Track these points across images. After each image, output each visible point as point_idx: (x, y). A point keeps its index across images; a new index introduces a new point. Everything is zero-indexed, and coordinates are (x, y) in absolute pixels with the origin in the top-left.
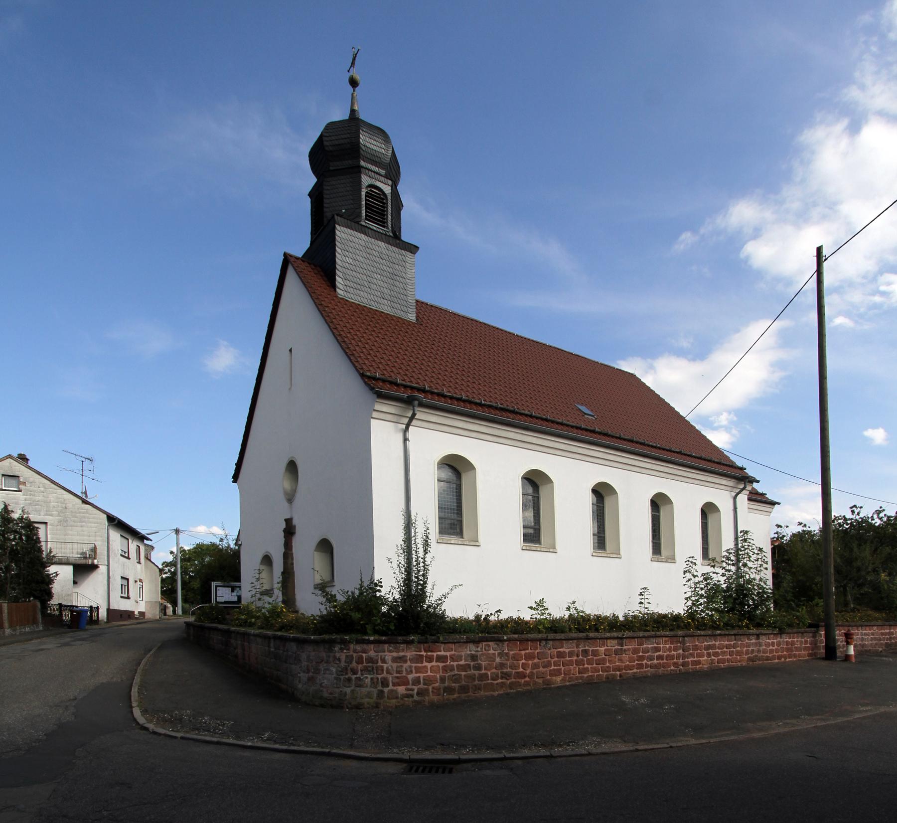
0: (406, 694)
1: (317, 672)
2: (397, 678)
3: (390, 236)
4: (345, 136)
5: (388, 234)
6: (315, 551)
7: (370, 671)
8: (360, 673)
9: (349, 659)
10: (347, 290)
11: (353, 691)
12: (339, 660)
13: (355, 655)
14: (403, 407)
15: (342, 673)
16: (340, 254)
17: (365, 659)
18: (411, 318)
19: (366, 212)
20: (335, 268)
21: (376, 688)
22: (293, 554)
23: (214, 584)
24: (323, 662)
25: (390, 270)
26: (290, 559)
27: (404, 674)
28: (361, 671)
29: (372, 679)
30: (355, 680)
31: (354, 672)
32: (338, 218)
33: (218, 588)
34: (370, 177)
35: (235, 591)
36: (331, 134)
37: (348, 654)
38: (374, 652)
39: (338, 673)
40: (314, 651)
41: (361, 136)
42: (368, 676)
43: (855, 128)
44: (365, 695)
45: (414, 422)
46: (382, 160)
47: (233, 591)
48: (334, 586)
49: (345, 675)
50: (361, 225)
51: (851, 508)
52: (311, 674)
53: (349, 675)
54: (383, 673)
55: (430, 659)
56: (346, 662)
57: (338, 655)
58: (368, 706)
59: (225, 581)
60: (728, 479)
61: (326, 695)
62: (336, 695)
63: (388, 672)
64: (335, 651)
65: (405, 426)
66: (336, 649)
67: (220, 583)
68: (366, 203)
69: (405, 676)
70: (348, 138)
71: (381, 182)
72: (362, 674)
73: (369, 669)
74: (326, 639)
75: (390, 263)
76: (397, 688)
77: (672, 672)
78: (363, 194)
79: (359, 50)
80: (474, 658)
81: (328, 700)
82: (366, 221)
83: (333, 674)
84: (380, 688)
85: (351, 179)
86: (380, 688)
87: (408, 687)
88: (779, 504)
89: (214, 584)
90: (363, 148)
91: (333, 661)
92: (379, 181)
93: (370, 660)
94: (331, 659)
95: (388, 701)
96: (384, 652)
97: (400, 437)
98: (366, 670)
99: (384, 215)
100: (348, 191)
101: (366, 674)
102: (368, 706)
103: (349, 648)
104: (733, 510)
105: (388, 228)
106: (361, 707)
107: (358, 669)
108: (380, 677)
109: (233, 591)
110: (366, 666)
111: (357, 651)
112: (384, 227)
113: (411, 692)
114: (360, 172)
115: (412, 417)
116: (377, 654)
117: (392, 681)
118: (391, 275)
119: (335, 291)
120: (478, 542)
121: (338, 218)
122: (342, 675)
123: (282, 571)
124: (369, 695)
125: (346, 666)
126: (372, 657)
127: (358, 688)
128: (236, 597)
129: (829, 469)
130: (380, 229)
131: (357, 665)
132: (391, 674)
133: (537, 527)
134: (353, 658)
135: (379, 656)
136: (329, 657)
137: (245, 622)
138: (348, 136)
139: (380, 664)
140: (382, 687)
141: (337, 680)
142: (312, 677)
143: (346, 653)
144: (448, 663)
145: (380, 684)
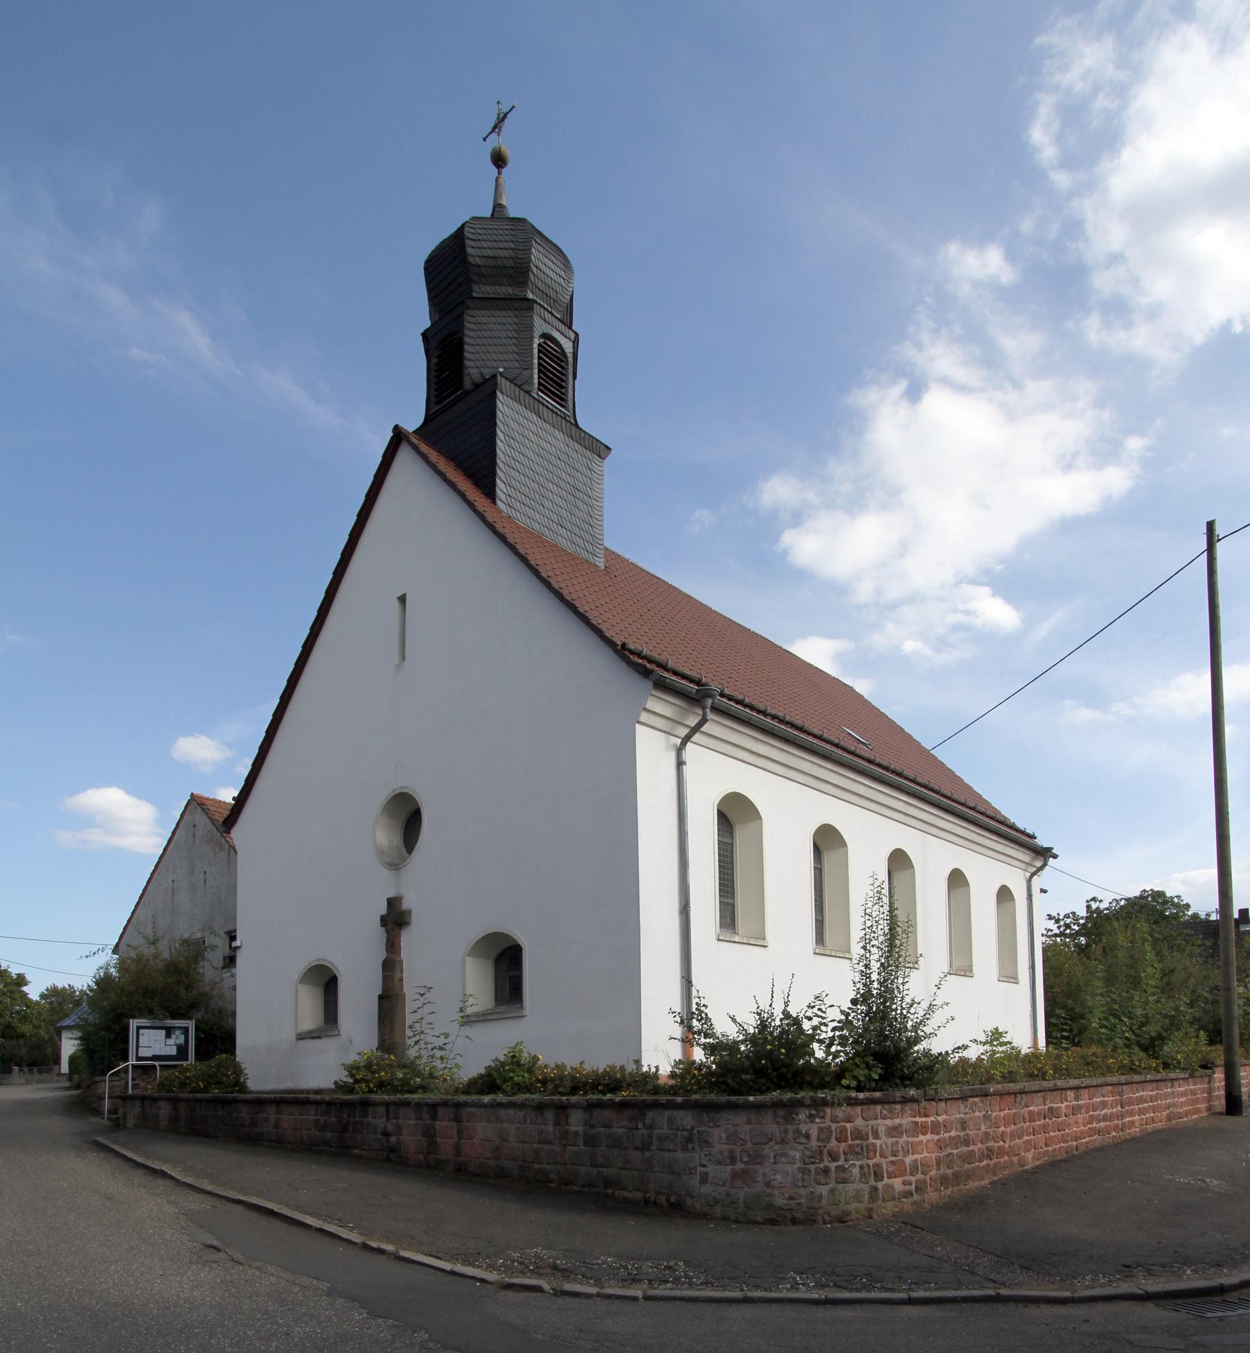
0: (904, 1190)
1: (758, 1161)
2: (893, 1163)
3: (572, 424)
4: (506, 245)
5: (568, 418)
6: (469, 955)
7: (858, 1153)
8: (842, 1158)
9: (825, 1134)
10: (511, 505)
11: (832, 1191)
12: (807, 1136)
13: (834, 1126)
14: (675, 705)
15: (813, 1160)
16: (502, 442)
17: (851, 1132)
18: (597, 564)
19: (539, 377)
20: (493, 463)
21: (868, 1183)
22: (402, 961)
23: (134, 1023)
24: (773, 1143)
25: (571, 481)
26: (398, 973)
27: (900, 1157)
28: (845, 1154)
29: (861, 1167)
30: (836, 1171)
31: (834, 1157)
33: (141, 1031)
34: (545, 320)
35: (173, 1036)
36: (480, 237)
37: (822, 1125)
38: (861, 1119)
39: (806, 1160)
40: (749, 1122)
41: (533, 249)
42: (856, 1162)
43: (915, 393)
44: (852, 1197)
45: (697, 737)
46: (560, 296)
47: (168, 1036)
48: (524, 1016)
49: (820, 1163)
51: (1087, 901)
52: (739, 1166)
53: (826, 1163)
54: (876, 1157)
55: (924, 1129)
56: (819, 1139)
57: (804, 1128)
58: (858, 1215)
59: (154, 1018)
60: (1026, 852)
61: (779, 1201)
62: (803, 1201)
63: (883, 1155)
64: (800, 1120)
65: (680, 740)
66: (800, 1117)
67: (145, 1021)
68: (539, 364)
69: (901, 1160)
70: (512, 249)
71: (559, 331)
72: (846, 1160)
73: (857, 1150)
74: (785, 1100)
75: (571, 469)
76: (893, 1182)
77: (1115, 1140)
78: (535, 346)
79: (513, 107)
80: (963, 1124)
81: (786, 1210)
82: (540, 393)
83: (796, 1164)
84: (872, 1182)
85: (514, 319)
86: (872, 1182)
87: (906, 1178)
89: (134, 1023)
90: (534, 269)
91: (795, 1140)
92: (557, 330)
93: (858, 1135)
94: (790, 1136)
95: (883, 1204)
96: (876, 1119)
97: (671, 758)
98: (852, 1152)
99: (562, 387)
100: (510, 338)
101: (852, 1160)
102: (858, 1215)
103: (825, 1113)
104: (1027, 898)
105: (569, 411)
106: (846, 1219)
107: (839, 1150)
108: (871, 1162)
109: (168, 1036)
110: (852, 1145)
111: (838, 1119)
112: (562, 406)
113: (908, 1187)
114: (531, 309)
115: (696, 729)
116: (866, 1123)
117: (887, 1170)
118: (572, 488)
119: (494, 502)
120: (765, 939)
122: (813, 1163)
123: (380, 992)
124: (857, 1197)
125: (820, 1147)
126: (860, 1128)
127: (841, 1185)
128: (175, 1048)
129: (1229, 837)
131: (838, 1144)
133: (820, 918)
134: (831, 1132)
135: (870, 1127)
136: (786, 1131)
137: (405, 1082)
138: (512, 245)
139: (871, 1140)
140: (875, 1181)
141: (803, 1173)
142: (745, 1171)
143: (819, 1123)
145: (873, 1176)
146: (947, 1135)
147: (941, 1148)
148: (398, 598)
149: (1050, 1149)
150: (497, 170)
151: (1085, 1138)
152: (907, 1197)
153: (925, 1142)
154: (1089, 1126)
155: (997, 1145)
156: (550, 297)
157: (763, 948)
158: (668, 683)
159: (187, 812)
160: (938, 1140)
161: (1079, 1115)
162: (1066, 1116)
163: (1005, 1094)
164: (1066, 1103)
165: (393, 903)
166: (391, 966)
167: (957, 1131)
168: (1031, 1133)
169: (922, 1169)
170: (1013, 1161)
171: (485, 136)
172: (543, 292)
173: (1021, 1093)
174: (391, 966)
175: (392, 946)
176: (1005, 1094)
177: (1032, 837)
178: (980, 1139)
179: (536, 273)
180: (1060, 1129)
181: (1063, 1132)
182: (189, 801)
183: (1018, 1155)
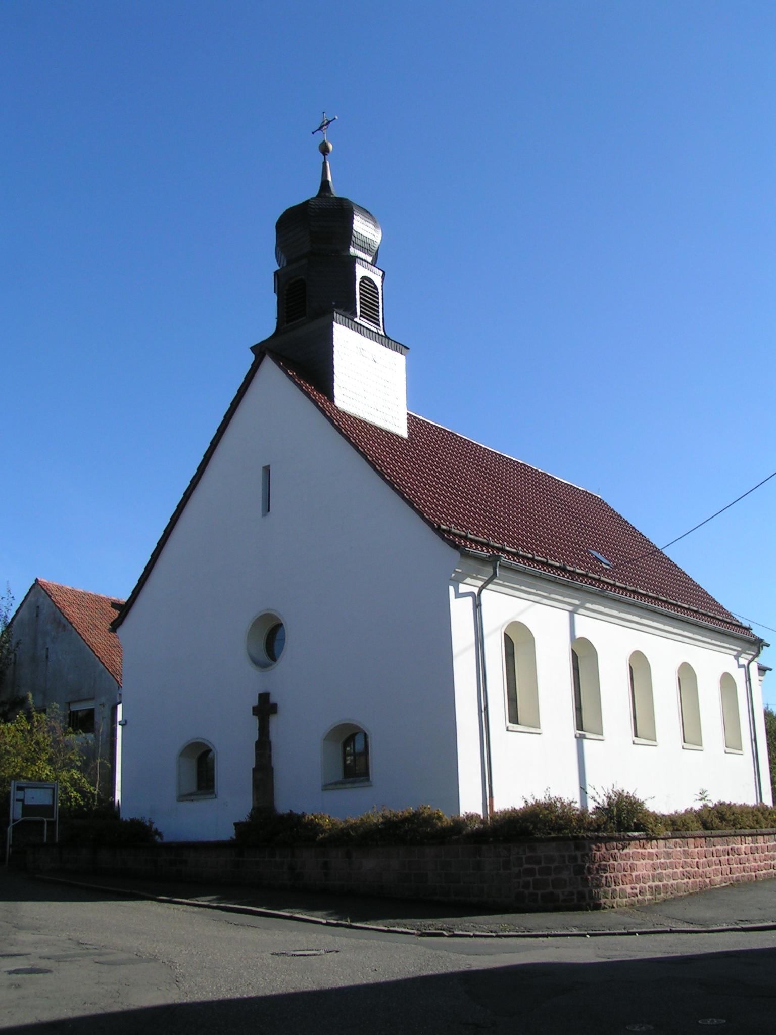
3: (382, 335)
32: (337, 316)
50: (356, 322)
55: (643, 857)
88: (771, 669)
108: (612, 875)
113: (634, 891)
121: (337, 316)
123: (254, 766)
130: (373, 327)
132: (620, 872)
144: (655, 861)
146: (658, 861)
147: (655, 869)
148: (263, 468)
149: (734, 876)
150: (323, 156)
151: (762, 870)
152: (634, 897)
153: (644, 864)
154: (765, 862)
155: (693, 870)
156: (365, 248)
157: (538, 735)
158: (471, 554)
159: (31, 594)
160: (653, 864)
161: (756, 854)
162: (746, 854)
163: (697, 837)
164: (744, 845)
165: (264, 698)
166: (263, 746)
167: (665, 859)
168: (718, 864)
169: (643, 881)
170: (706, 882)
171: (313, 131)
172: (363, 247)
173: (709, 837)
174: (263, 746)
175: (264, 730)
176: (697, 837)
177: (748, 629)
178: (681, 865)
179: (356, 236)
180: (741, 862)
181: (744, 865)
182: (34, 584)
183: (709, 878)
